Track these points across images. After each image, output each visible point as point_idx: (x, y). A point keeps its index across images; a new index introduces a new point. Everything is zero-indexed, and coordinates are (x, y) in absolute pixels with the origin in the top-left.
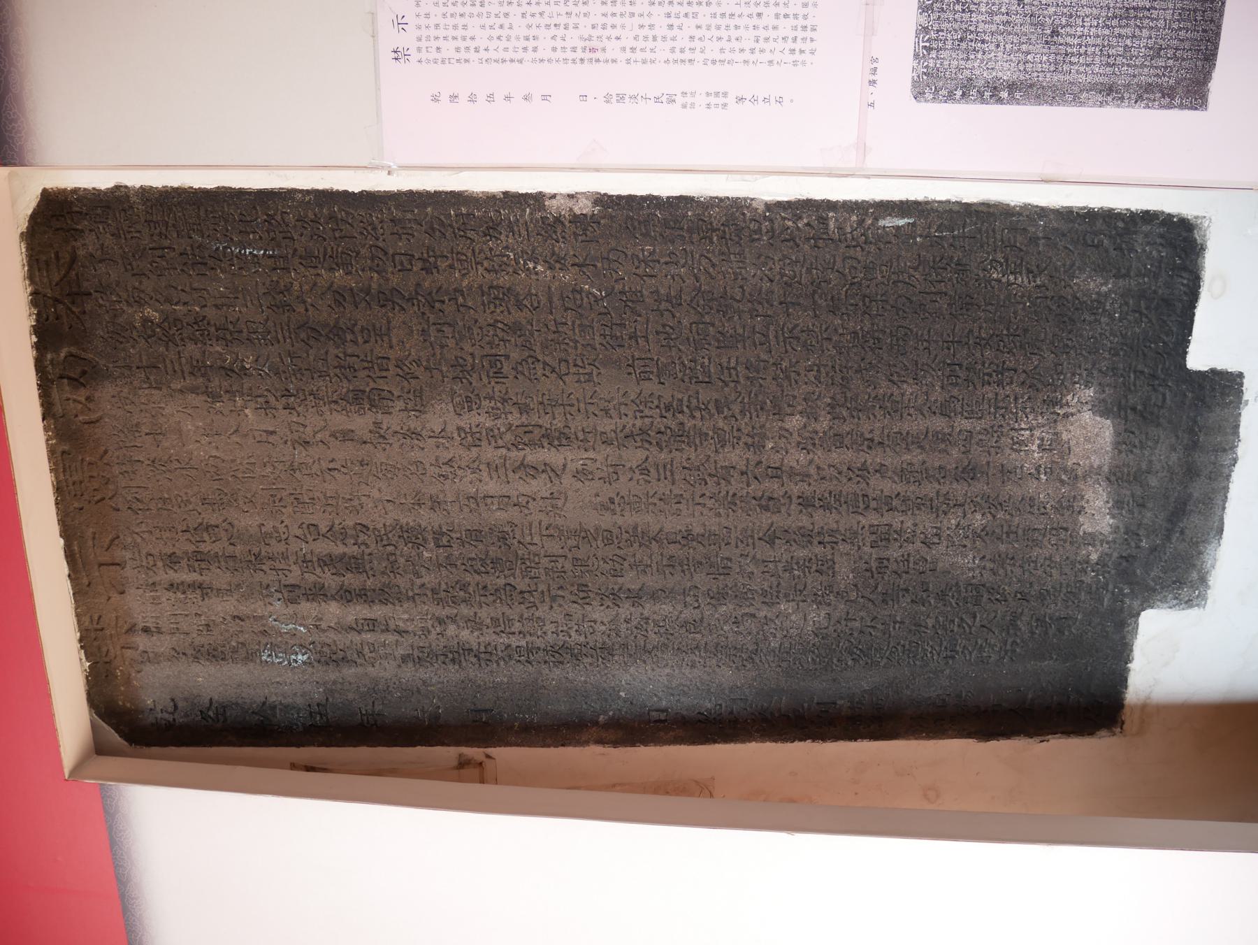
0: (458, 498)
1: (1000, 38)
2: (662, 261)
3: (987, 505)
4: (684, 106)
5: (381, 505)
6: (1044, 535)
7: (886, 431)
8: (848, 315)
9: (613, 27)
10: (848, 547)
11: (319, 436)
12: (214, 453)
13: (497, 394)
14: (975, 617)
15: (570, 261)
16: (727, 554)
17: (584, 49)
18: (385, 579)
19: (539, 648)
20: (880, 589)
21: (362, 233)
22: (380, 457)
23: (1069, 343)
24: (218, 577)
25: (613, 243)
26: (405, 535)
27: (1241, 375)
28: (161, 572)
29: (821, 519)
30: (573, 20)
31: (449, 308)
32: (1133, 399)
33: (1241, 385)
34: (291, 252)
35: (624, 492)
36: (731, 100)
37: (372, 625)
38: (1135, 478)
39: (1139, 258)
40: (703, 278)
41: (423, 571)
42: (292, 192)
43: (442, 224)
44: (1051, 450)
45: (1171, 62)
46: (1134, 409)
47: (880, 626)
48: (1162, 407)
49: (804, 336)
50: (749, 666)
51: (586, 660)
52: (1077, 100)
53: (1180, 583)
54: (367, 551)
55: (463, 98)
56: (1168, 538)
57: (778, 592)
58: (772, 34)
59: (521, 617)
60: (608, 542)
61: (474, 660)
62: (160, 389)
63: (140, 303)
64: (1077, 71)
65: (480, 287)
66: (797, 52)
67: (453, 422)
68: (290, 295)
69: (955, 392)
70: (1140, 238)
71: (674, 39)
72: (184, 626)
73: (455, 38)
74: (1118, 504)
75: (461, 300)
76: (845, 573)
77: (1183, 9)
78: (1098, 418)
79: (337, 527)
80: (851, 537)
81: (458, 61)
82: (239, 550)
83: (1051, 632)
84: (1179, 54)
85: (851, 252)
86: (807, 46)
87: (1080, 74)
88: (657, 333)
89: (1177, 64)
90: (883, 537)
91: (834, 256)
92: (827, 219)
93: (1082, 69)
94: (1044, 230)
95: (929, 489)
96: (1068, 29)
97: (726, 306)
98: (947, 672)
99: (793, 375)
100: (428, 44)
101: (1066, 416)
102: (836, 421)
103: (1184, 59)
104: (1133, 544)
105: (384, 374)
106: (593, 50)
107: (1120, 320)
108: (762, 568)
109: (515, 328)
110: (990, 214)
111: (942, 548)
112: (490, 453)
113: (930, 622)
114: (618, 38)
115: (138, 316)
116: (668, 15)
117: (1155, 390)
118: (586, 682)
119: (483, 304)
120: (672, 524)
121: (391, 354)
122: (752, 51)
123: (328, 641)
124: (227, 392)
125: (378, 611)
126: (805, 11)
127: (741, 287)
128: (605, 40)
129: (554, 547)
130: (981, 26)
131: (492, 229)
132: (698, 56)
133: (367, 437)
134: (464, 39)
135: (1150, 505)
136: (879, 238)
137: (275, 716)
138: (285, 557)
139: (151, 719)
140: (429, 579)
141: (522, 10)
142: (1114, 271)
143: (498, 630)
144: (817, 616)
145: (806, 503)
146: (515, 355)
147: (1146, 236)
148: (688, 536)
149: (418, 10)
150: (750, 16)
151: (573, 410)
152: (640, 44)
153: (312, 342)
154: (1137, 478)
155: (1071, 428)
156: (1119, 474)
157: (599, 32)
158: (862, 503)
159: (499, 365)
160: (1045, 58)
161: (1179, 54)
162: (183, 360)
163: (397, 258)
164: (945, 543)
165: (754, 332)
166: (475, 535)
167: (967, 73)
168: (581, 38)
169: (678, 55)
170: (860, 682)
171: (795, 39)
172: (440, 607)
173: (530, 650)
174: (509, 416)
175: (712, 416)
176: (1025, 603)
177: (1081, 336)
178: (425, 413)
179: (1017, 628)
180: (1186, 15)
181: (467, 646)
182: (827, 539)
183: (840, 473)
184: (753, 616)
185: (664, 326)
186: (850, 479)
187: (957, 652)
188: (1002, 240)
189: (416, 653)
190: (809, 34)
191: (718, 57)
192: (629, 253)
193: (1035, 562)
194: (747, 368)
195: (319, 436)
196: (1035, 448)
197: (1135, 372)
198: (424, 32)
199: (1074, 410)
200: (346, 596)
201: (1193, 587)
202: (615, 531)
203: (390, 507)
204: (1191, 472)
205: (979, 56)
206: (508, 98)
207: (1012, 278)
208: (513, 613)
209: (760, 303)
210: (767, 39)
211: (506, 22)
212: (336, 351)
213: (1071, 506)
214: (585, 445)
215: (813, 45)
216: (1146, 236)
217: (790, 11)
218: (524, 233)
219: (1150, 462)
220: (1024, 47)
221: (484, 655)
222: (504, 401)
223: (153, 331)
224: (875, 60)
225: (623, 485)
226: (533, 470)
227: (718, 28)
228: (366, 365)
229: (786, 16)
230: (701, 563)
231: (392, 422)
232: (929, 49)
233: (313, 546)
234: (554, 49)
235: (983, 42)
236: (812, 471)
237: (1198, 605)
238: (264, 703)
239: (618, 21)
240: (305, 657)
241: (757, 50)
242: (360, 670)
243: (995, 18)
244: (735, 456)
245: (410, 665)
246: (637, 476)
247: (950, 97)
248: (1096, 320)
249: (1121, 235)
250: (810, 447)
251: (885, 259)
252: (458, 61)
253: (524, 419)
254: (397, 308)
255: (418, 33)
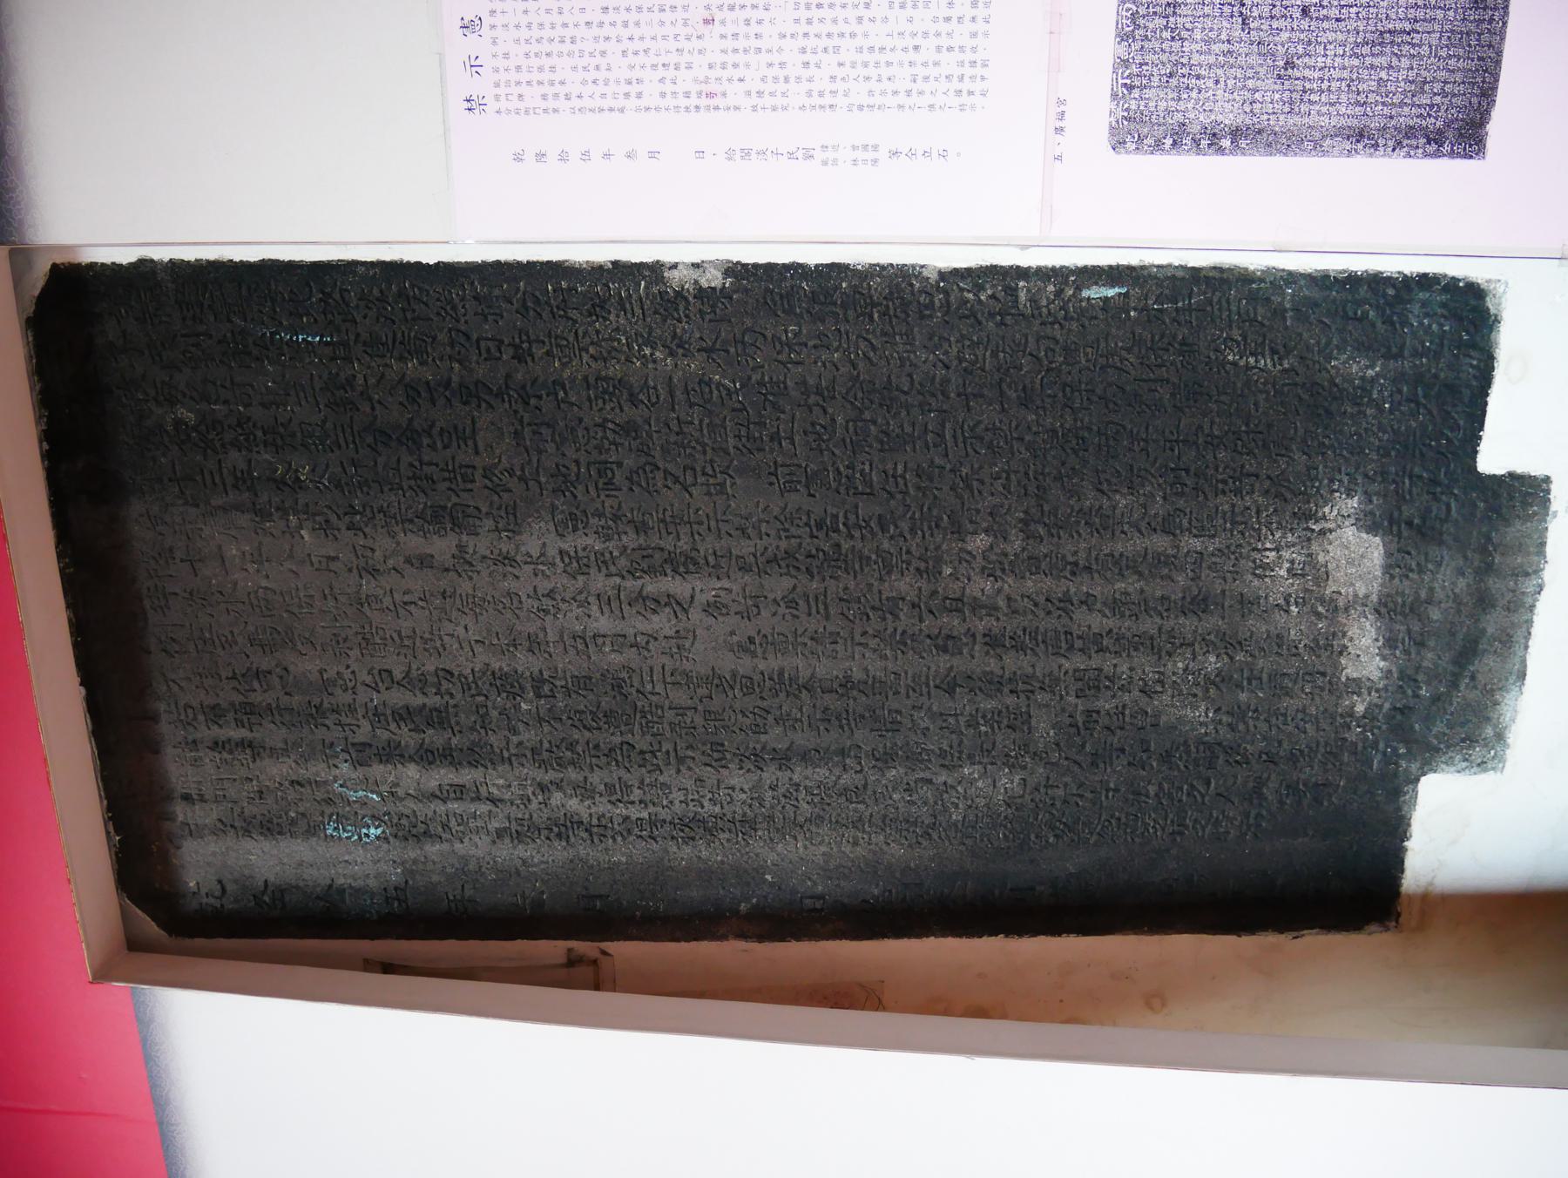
0: (562, 637)
1: (1220, 72)
2: (811, 343)
3: (1222, 645)
4: (825, 163)
5: (467, 645)
6: (1295, 682)
7: (1094, 554)
8: (1044, 408)
9: (735, 66)
10: (1048, 696)
11: (391, 563)
12: (264, 583)
13: (608, 510)
14: (1208, 784)
15: (695, 345)
16: (895, 706)
17: (700, 94)
18: (474, 736)
19: (664, 821)
20: (1088, 748)
21: (438, 314)
22: (465, 587)
23: (1327, 442)
24: (271, 733)
25: (748, 322)
26: (498, 683)
27: (1547, 480)
28: (203, 727)
29: (1013, 662)
30: (686, 58)
31: (547, 405)
32: (1407, 511)
33: (1548, 491)
34: (352, 337)
35: (766, 630)
36: (883, 154)
37: (459, 791)
38: (1412, 610)
39: (1414, 334)
40: (861, 365)
41: (521, 726)
42: (354, 264)
43: (537, 301)
44: (1303, 576)
45: (1438, 99)
46: (1409, 524)
47: (1089, 795)
48: (1446, 520)
49: (988, 436)
50: (925, 843)
51: (722, 836)
52: (1318, 148)
53: (1471, 740)
54: (452, 702)
55: (552, 157)
56: (1454, 685)
57: (960, 752)
58: (932, 71)
59: (642, 782)
60: (748, 690)
61: (585, 835)
62: (197, 506)
63: (172, 402)
64: (1319, 113)
65: (586, 378)
66: (965, 93)
67: (554, 545)
68: (353, 390)
69: (1181, 503)
70: (1416, 309)
71: (810, 80)
72: (232, 793)
73: (540, 83)
74: (1390, 643)
75: (561, 394)
76: (1044, 729)
77: (1452, 31)
78: (1364, 535)
79: (414, 673)
80: (1050, 684)
81: (545, 111)
82: (296, 700)
83: (1305, 802)
84: (1448, 88)
85: (1048, 330)
86: (978, 86)
87: (1321, 116)
88: (805, 433)
89: (1446, 101)
90: (1091, 684)
91: (1026, 336)
92: (1016, 289)
93: (1324, 109)
94: (1292, 301)
95: (1149, 625)
96: (1306, 60)
97: (891, 399)
98: (1174, 852)
99: (975, 483)
100: (508, 90)
101: (1322, 532)
102: (1031, 541)
103: (1454, 95)
104: (1410, 692)
105: (469, 486)
106: (710, 95)
107: (1391, 411)
108: (940, 723)
109: (629, 429)
110: (1223, 281)
111: (1166, 698)
112: (600, 582)
113: (1152, 790)
114: (741, 80)
115: (170, 418)
116: (803, 50)
117: (1436, 499)
118: (722, 862)
119: (589, 399)
120: (826, 669)
121: (477, 461)
122: (909, 93)
123: (406, 812)
124: (278, 509)
125: (467, 776)
126: (974, 42)
127: (910, 375)
128: (725, 83)
129: (680, 697)
130: (1196, 57)
131: (598, 307)
132: (840, 100)
133: (449, 563)
134: (552, 83)
135: (1432, 643)
136: (1082, 312)
137: (343, 901)
138: (351, 709)
139: (194, 905)
140: (528, 736)
141: (622, 47)
142: (1383, 350)
143: (613, 798)
144: (1009, 782)
145: (993, 642)
146: (629, 462)
147: (1424, 304)
148: (847, 683)
149: (495, 49)
150: (905, 50)
151: (703, 529)
152: (769, 87)
153: (380, 448)
154: (1414, 609)
155: (1330, 548)
156: (1391, 605)
157: (718, 72)
158: (1065, 642)
159: (610, 474)
160: (1277, 96)
161: (1448, 88)
162: (225, 471)
163: (483, 344)
164: (1170, 692)
165: (926, 431)
166: (583, 683)
167: (1179, 117)
168: (696, 80)
169: (816, 100)
170: (1065, 862)
171: (961, 78)
172: (542, 770)
173: (654, 822)
174: (624, 537)
175: (873, 534)
176: (1272, 766)
177: (1341, 432)
178: (520, 533)
179: (1261, 796)
180: (1457, 37)
181: (576, 818)
182: (1021, 686)
183: (1036, 605)
184: (930, 781)
185: (813, 424)
186: (1049, 613)
187: (1186, 827)
188: (1239, 314)
189: (514, 826)
190: (979, 71)
191: (866, 101)
192: (769, 335)
193: (1285, 715)
194: (918, 476)
195: (391, 563)
196: (1283, 573)
197: (1411, 477)
198: (503, 77)
199: (1332, 526)
200: (427, 757)
201: (1487, 745)
202: (757, 678)
203: (478, 649)
204: (1484, 601)
205: (1194, 94)
206: (607, 156)
207: (1252, 360)
208: (632, 778)
209: (933, 395)
210: (926, 78)
211: (603, 62)
212: (410, 459)
213: (1330, 646)
214: (717, 571)
215: (984, 85)
216: (1424, 304)
217: (955, 43)
218: (638, 311)
219: (1431, 589)
220: (1250, 83)
221: (598, 830)
222: (616, 518)
223: (189, 436)
224: (1061, 102)
225: (766, 621)
226: (656, 603)
227: (866, 65)
228: (446, 475)
229: (950, 49)
230: (863, 717)
231: (481, 544)
232: (1130, 88)
233: (386, 695)
234: (663, 95)
235: (1198, 77)
236: (1001, 603)
237: (1493, 769)
238: (330, 886)
239: (740, 58)
240: (379, 831)
241: (914, 92)
242: (445, 846)
243: (1213, 47)
244: (904, 585)
245: (507, 840)
246: (782, 610)
247: (1158, 146)
248: (1360, 412)
249: (1391, 305)
250: (999, 573)
251: (1090, 338)
252: (545, 111)
253: (641, 541)
254: (484, 405)
255: (496, 77)
